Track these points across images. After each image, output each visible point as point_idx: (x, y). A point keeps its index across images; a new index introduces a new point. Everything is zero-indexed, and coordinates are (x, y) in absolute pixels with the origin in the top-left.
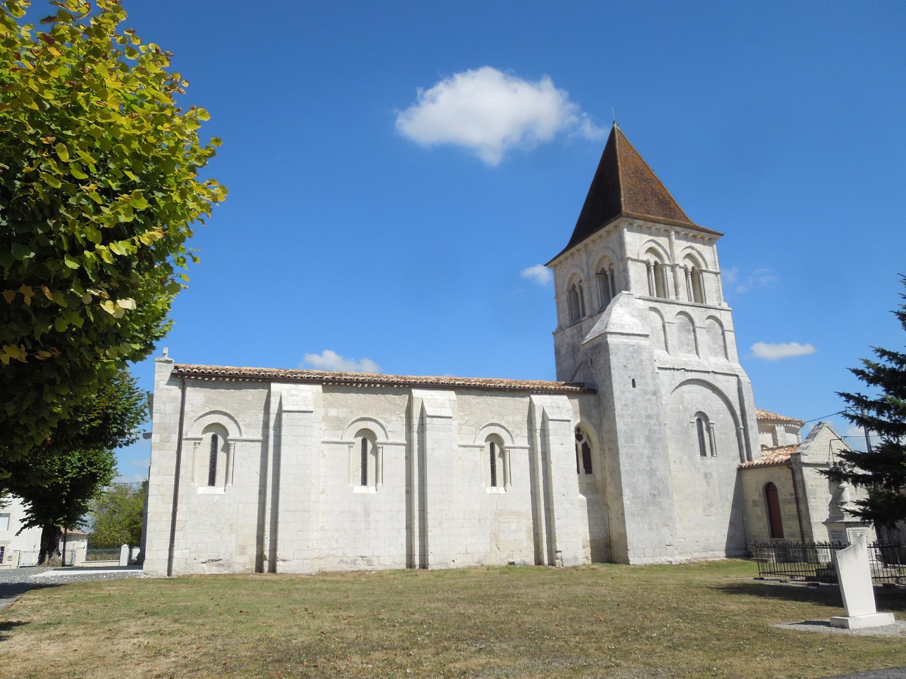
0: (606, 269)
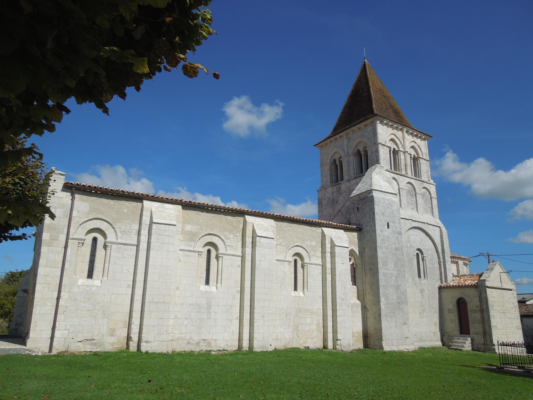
0: (361, 149)
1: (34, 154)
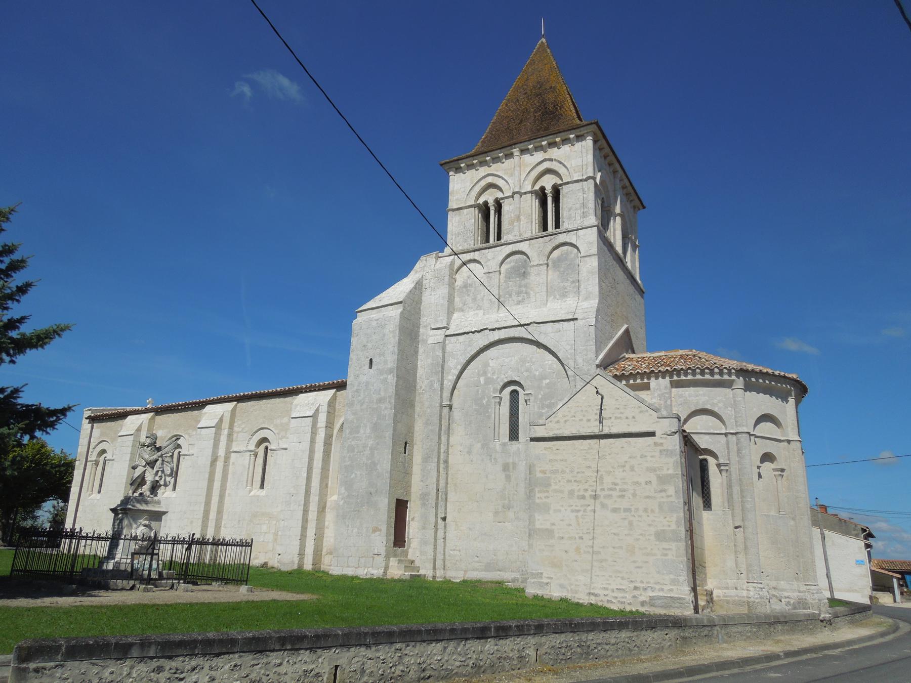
1: (14, 334)
